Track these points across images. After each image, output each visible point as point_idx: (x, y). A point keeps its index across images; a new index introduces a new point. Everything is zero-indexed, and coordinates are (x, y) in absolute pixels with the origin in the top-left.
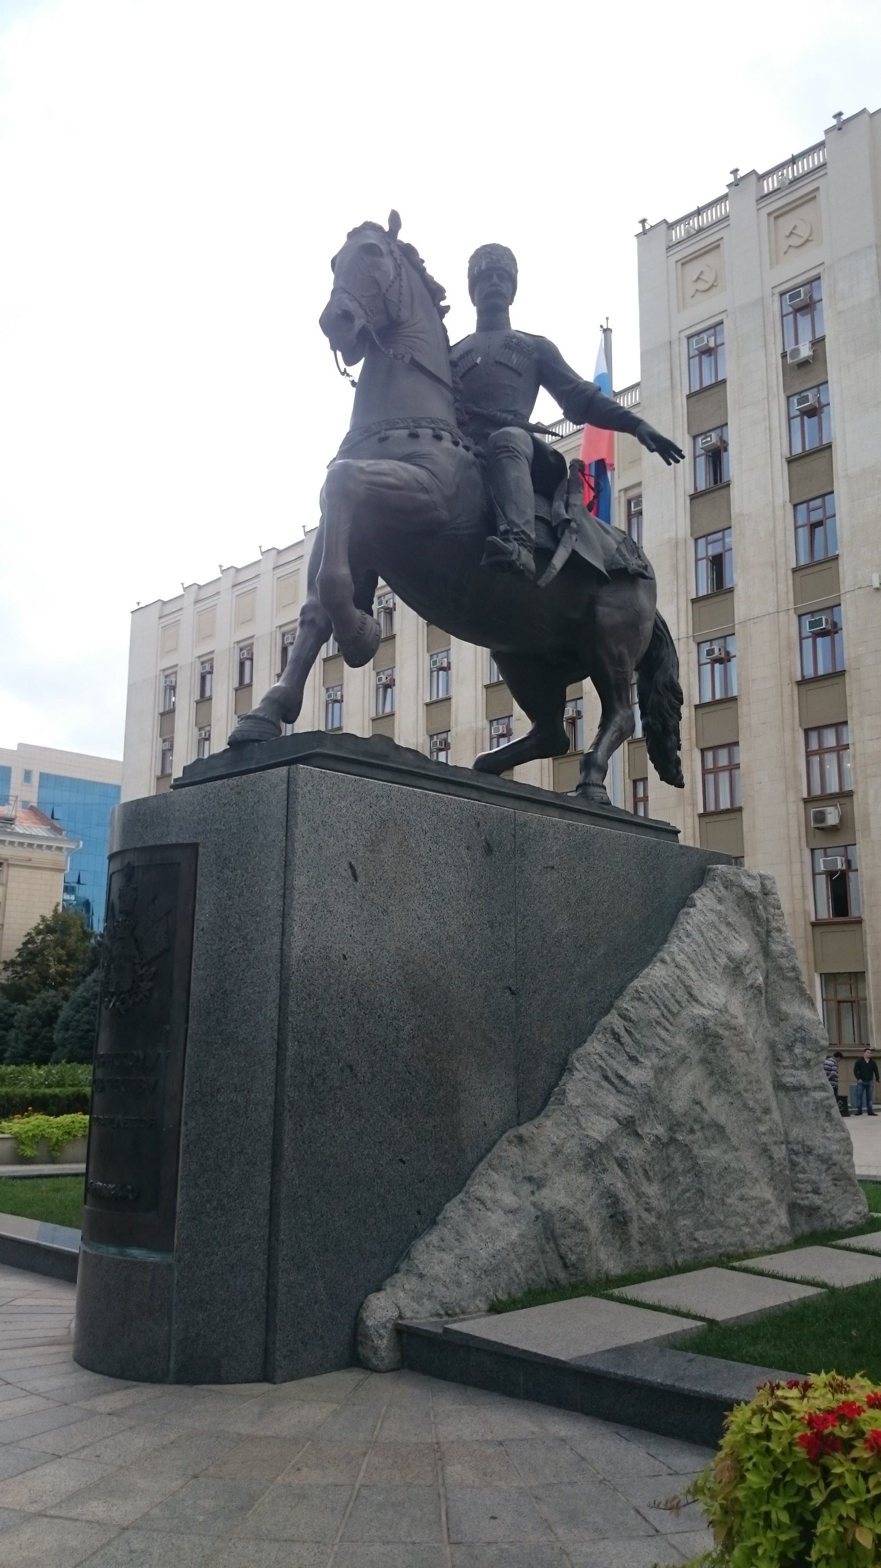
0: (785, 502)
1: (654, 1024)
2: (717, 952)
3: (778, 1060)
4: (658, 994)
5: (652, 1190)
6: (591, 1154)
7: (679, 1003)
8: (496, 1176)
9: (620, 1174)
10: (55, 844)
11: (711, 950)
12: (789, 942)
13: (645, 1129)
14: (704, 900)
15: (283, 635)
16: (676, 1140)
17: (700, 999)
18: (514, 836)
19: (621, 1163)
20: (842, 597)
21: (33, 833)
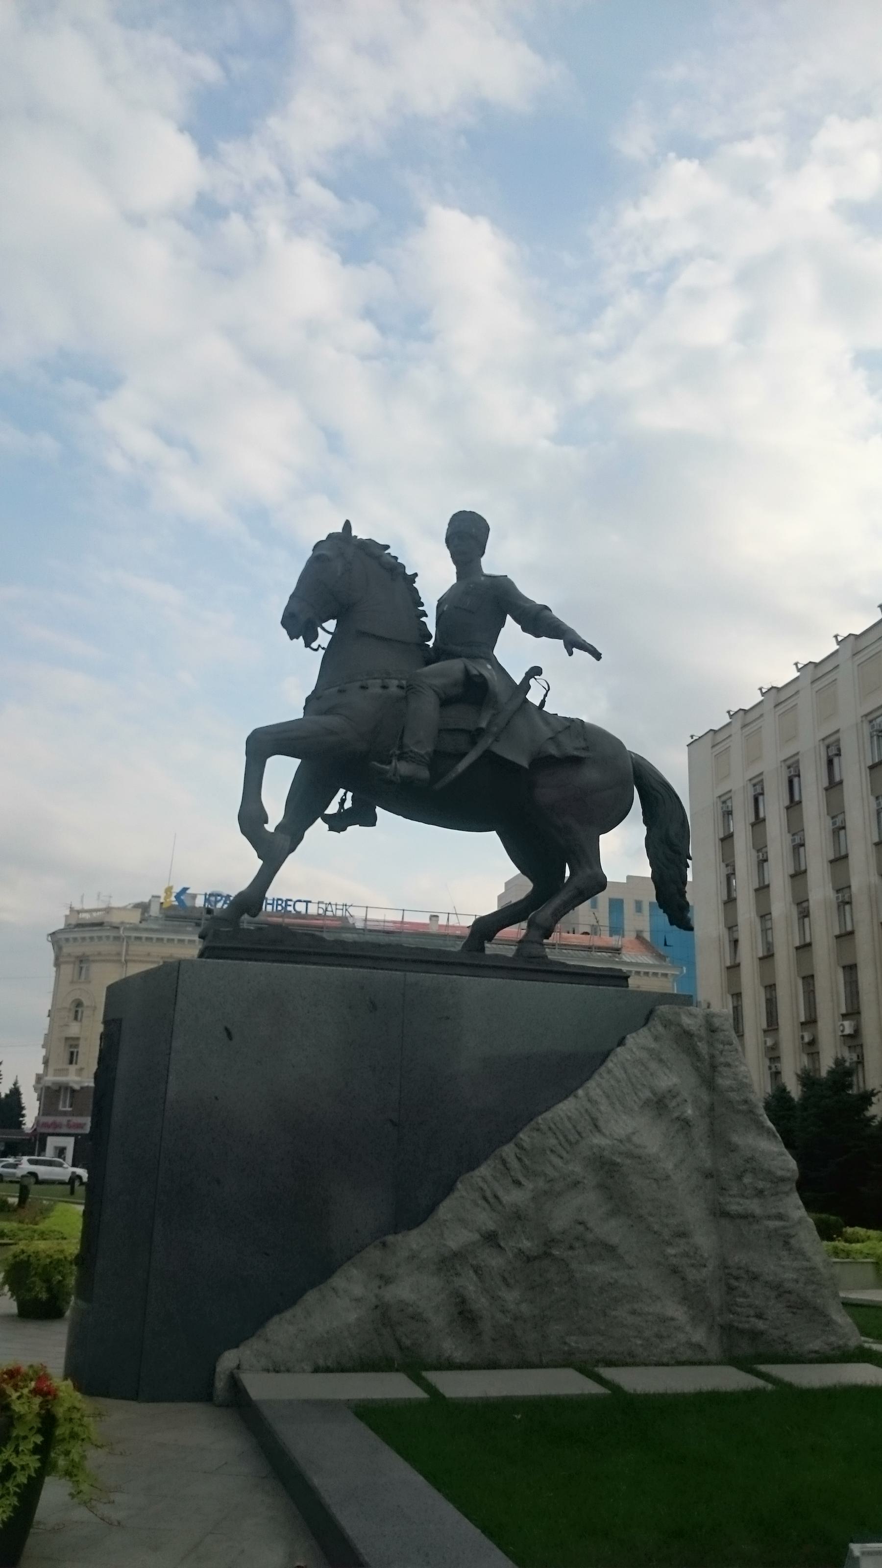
1: (548, 1152)
2: (639, 1087)
3: (723, 1189)
5: (511, 1296)
7: (579, 1133)
8: (355, 1272)
9: (475, 1278)
10: (660, 971)
11: (632, 1085)
15: (828, 747)
16: (550, 1255)
17: (604, 1131)
19: (477, 1270)
21: (639, 961)
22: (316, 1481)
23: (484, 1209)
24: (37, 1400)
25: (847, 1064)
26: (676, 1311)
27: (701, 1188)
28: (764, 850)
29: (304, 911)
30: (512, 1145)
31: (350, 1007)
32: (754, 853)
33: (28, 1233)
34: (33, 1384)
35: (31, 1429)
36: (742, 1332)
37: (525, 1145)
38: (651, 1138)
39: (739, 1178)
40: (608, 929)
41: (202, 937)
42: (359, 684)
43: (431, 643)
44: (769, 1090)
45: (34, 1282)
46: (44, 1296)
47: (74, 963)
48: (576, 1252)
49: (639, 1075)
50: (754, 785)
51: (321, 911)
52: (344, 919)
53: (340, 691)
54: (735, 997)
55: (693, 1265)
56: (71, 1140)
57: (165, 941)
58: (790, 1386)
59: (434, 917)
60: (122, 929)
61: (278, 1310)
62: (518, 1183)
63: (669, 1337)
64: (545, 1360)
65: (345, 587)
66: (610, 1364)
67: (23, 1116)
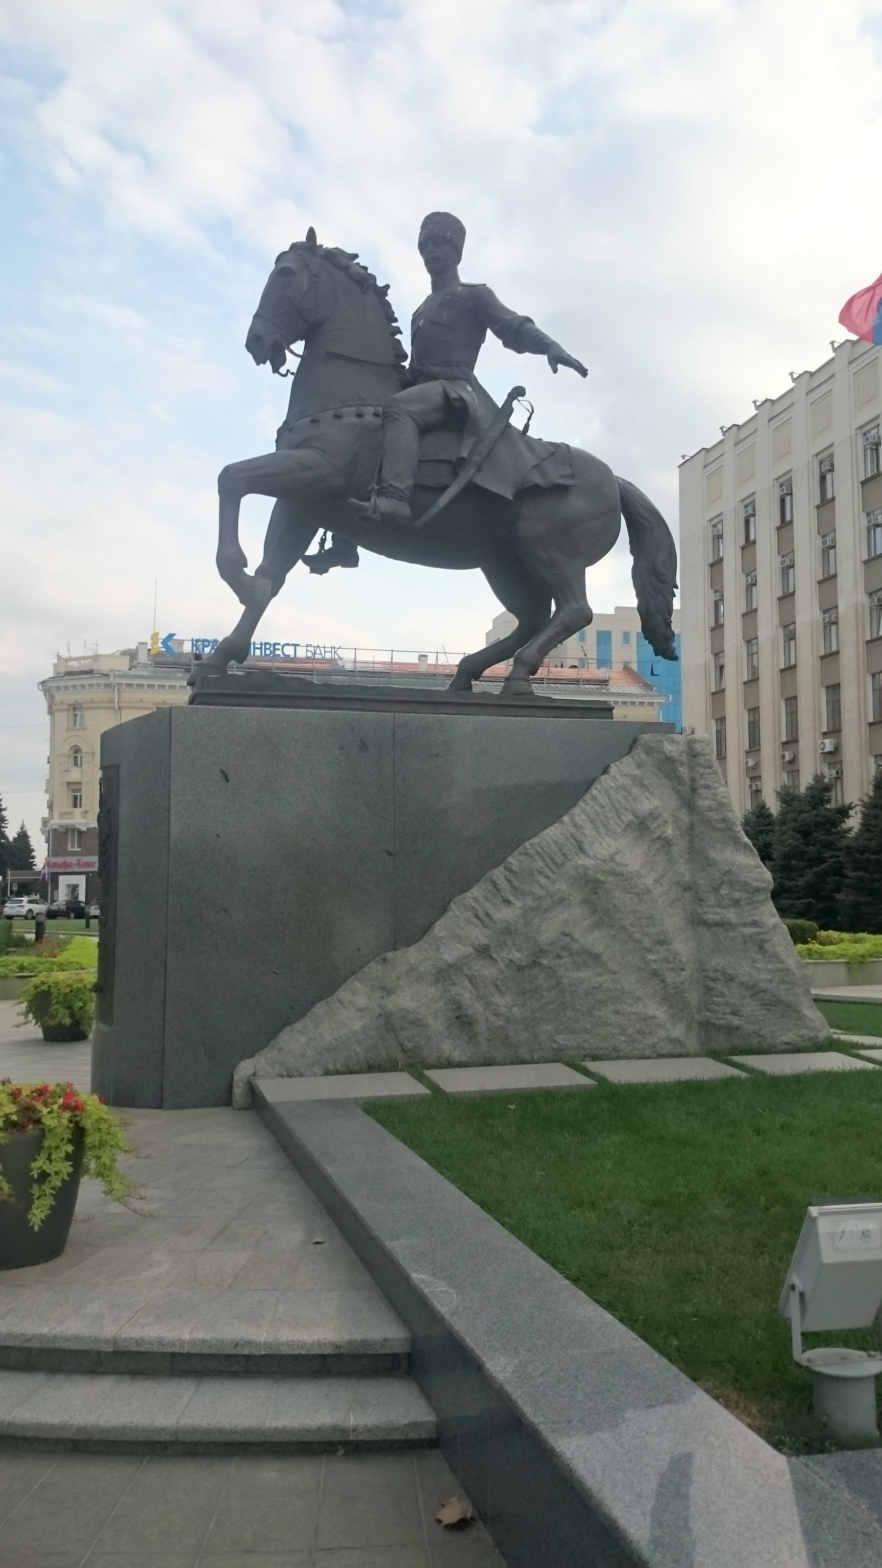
1: (536, 874)
3: (701, 900)
4: (546, 849)
5: (503, 1002)
6: (440, 971)
7: (565, 856)
8: (359, 984)
10: (646, 700)
11: (616, 809)
12: (719, 797)
15: (821, 463)
16: (540, 964)
17: (589, 852)
18: (394, 735)
19: (471, 979)
22: (330, 1170)
23: (476, 925)
24: (67, 1115)
25: (826, 780)
26: (659, 1012)
27: (680, 899)
28: (753, 574)
29: (292, 655)
30: (501, 868)
31: (342, 748)
32: (743, 577)
33: (47, 965)
34: (61, 1101)
35: (63, 1139)
36: (718, 1028)
37: (513, 868)
38: (632, 857)
39: (716, 890)
40: (596, 661)
41: (191, 684)
42: (332, 412)
43: (406, 364)
44: (749, 807)
45: (57, 1010)
46: (68, 1021)
47: (68, 710)
48: (563, 961)
49: (622, 801)
50: (746, 506)
51: (310, 654)
52: (332, 661)
53: (313, 421)
54: (719, 721)
55: (672, 969)
56: (83, 877)
57: (156, 688)
58: (763, 1074)
59: (423, 657)
60: (112, 676)
61: (289, 1023)
62: (507, 902)
63: (650, 1033)
64: (536, 1057)
65: (312, 303)
66: (595, 1058)
67: (33, 857)
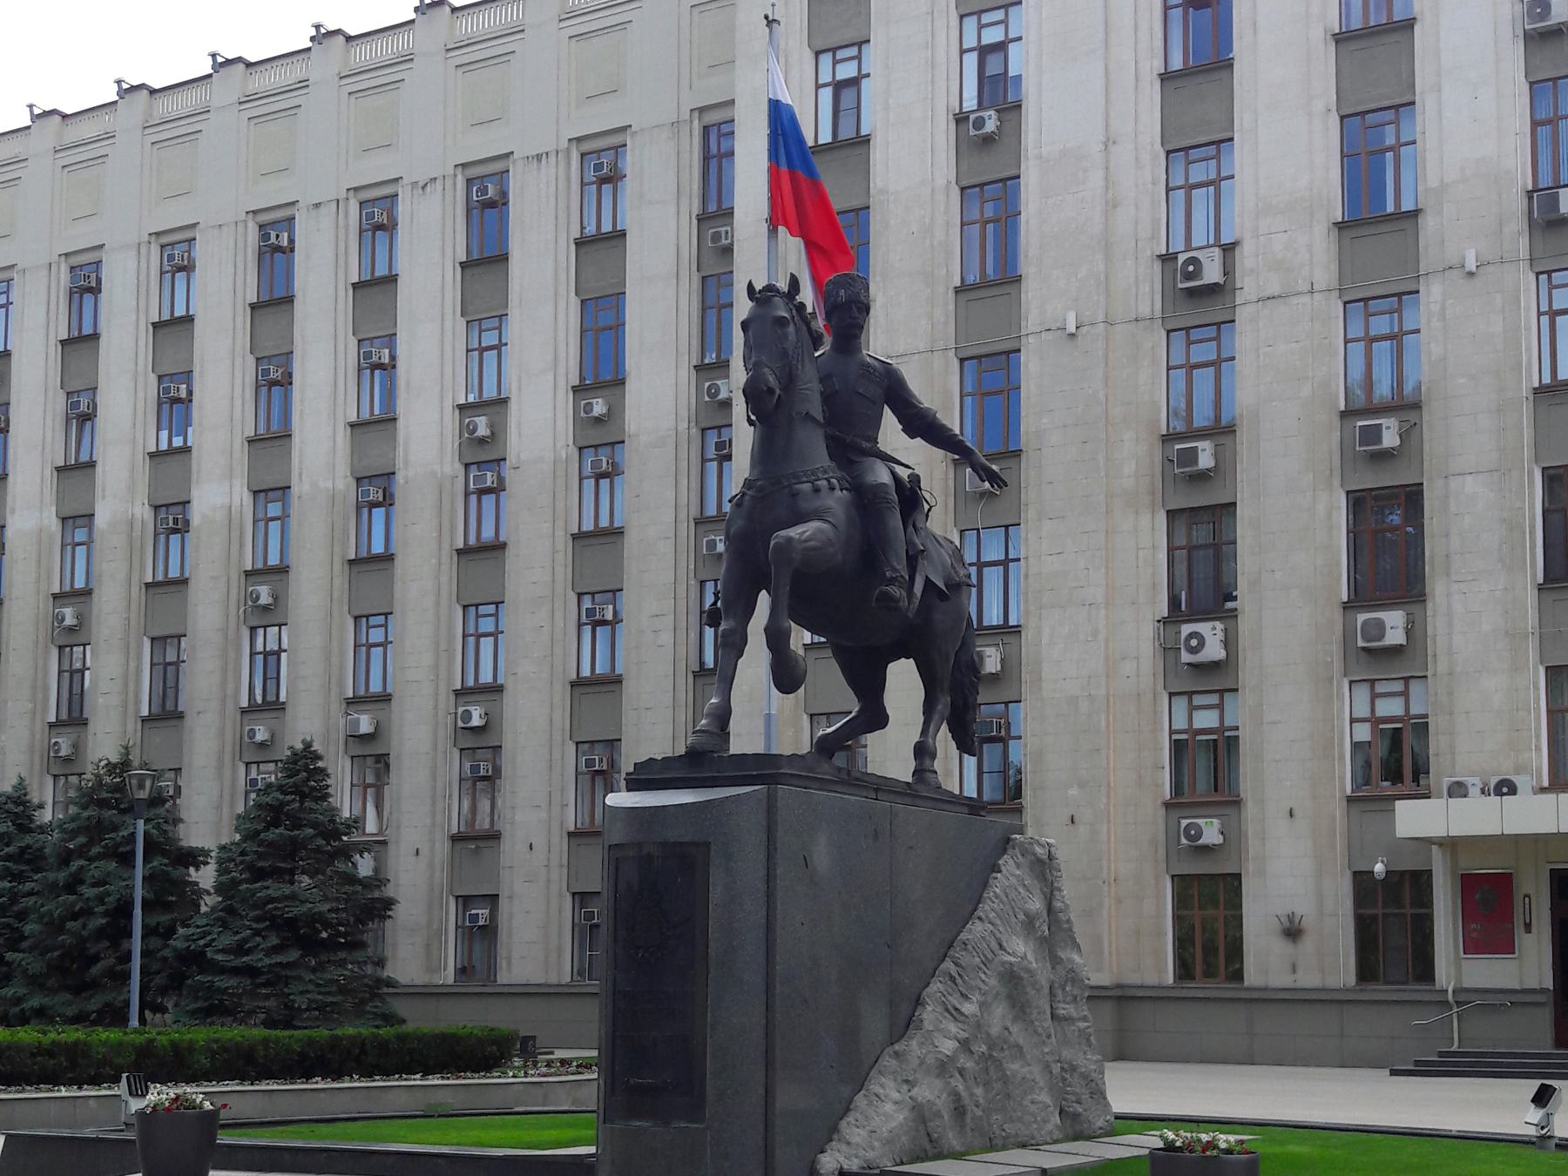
0: (949, 182)
13: (975, 1048)
14: (1007, 863)
19: (961, 1072)
20: (1023, 340)
